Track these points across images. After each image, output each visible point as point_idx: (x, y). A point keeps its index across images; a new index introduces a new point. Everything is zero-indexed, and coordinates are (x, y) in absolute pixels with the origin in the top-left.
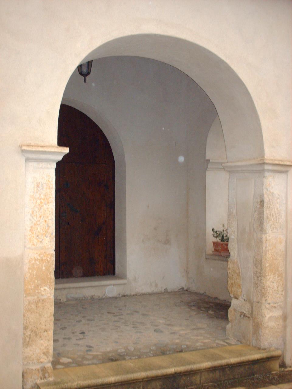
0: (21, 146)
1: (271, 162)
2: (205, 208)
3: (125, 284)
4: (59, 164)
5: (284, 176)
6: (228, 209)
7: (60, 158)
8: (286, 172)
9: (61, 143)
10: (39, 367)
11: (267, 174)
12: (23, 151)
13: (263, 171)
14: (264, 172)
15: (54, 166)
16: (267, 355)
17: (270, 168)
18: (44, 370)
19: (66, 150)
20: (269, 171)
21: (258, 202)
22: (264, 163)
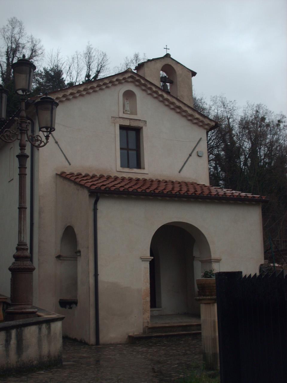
0: (141, 257)
1: (213, 259)
2: (184, 66)
3: (161, 310)
4: (150, 262)
5: (218, 263)
6: (129, 114)
7: (151, 260)
8: (219, 262)
9: (151, 256)
10: (147, 321)
11: (212, 263)
12: (141, 259)
13: (211, 262)
14: (212, 264)
15: (149, 262)
16: (127, 120)
17: (213, 261)
18: (148, 322)
19: (152, 258)
20: (213, 262)
21: (205, 270)
22: (211, 260)
